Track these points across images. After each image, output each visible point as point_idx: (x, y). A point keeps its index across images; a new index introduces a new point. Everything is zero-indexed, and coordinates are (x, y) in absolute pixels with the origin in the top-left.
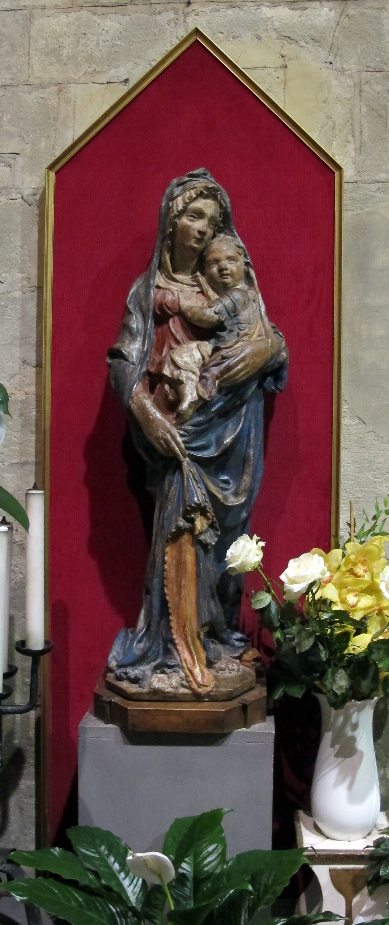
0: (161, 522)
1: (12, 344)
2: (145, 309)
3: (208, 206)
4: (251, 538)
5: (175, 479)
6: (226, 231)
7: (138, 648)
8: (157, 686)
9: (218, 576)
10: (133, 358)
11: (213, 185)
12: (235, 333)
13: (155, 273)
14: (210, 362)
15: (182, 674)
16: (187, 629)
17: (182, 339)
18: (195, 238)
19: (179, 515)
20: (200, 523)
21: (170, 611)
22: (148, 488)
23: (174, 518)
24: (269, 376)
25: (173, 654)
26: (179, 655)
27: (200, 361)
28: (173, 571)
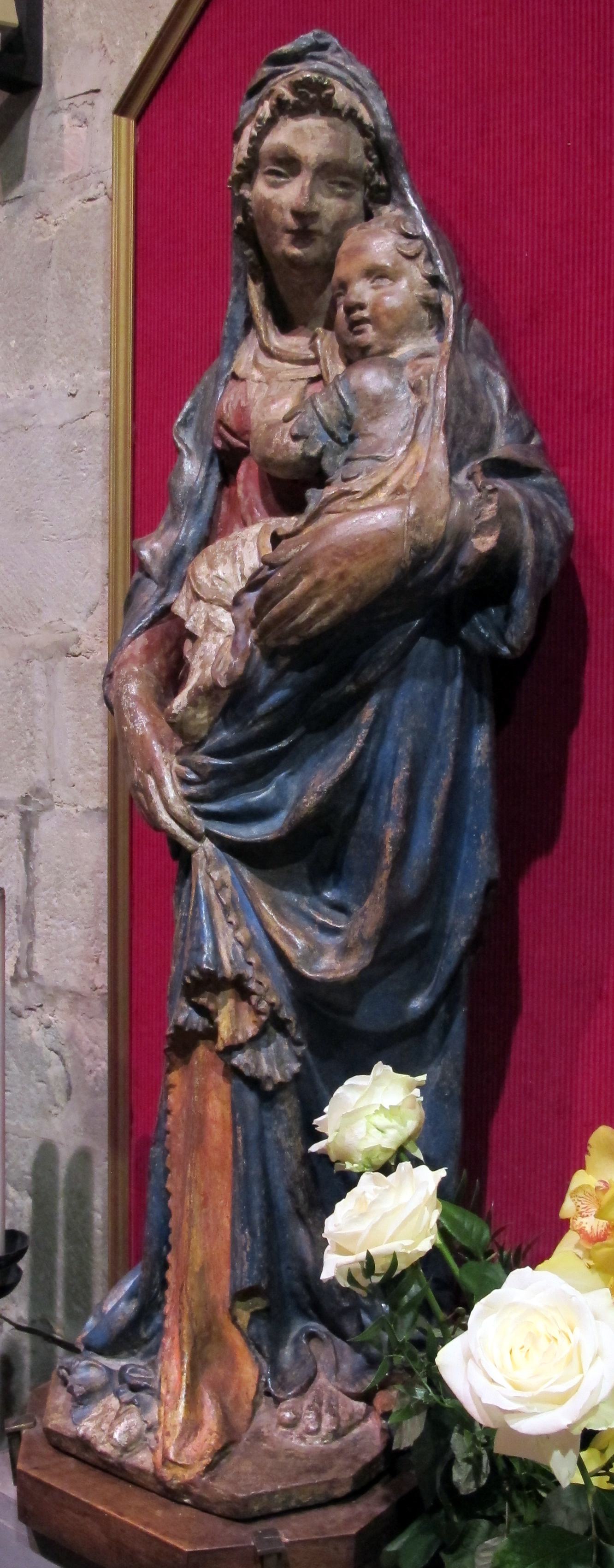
1: (90, 536)
20: (232, 1021)
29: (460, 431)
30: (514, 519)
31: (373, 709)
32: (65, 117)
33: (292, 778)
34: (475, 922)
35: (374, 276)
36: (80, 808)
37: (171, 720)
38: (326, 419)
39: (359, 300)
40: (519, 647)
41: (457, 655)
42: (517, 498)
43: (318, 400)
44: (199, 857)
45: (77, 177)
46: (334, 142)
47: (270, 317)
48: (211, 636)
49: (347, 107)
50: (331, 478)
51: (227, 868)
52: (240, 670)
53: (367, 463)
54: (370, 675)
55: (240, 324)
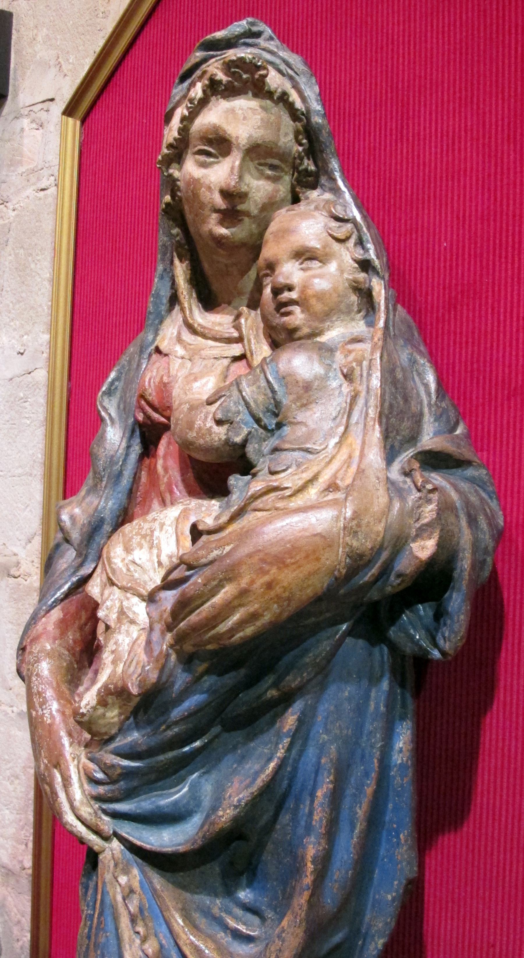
1: (31, 475)
29: (393, 420)
30: (452, 519)
31: (295, 717)
32: (25, 122)
33: (206, 776)
34: (393, 924)
36: (15, 709)
37: (78, 718)
38: (252, 404)
39: (288, 282)
40: (451, 652)
41: (382, 653)
42: (454, 495)
43: (244, 384)
44: (105, 858)
45: (33, 171)
46: (266, 124)
47: (194, 295)
48: (124, 628)
49: (280, 90)
50: (257, 469)
51: (135, 871)
52: (153, 677)
53: (296, 454)
54: (293, 681)
55: (165, 301)
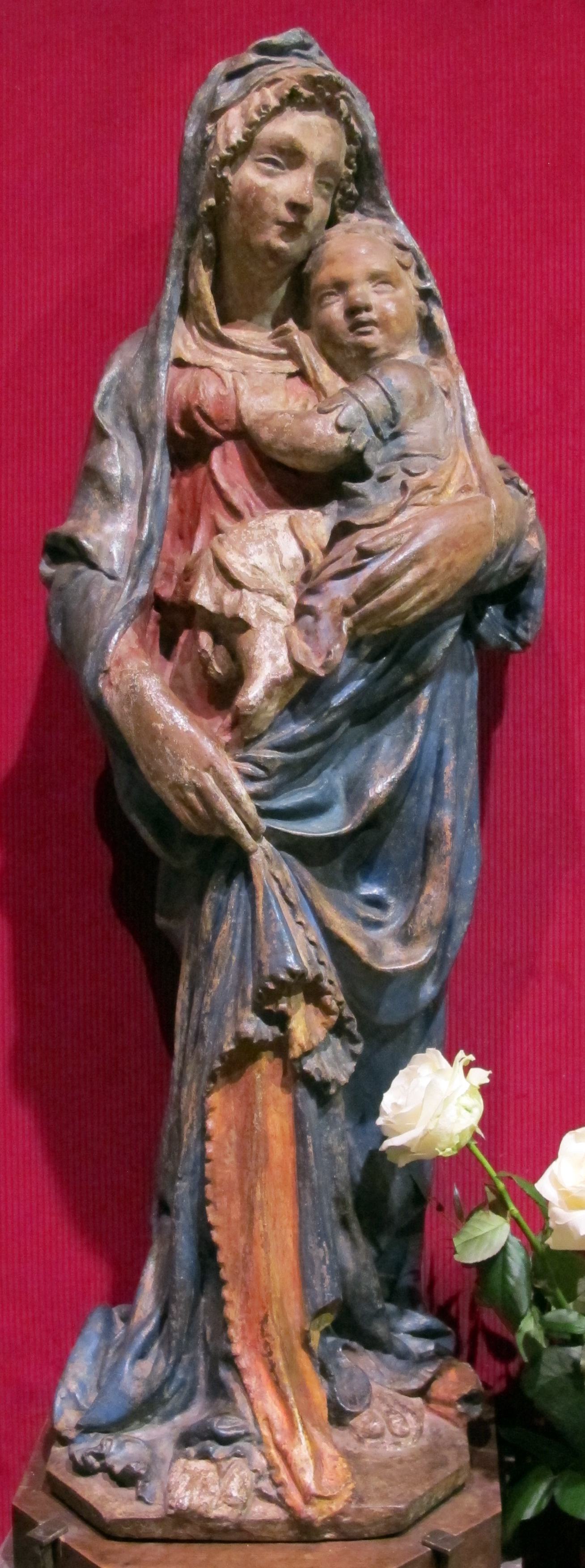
0: (194, 1021)
2: (143, 426)
3: (313, 132)
4: (451, 1060)
5: (233, 901)
6: (366, 205)
7: (136, 1376)
8: (186, 1503)
9: (360, 1160)
10: (112, 560)
11: (327, 73)
12: (396, 481)
13: (172, 326)
14: (325, 567)
15: (260, 1461)
16: (271, 1328)
17: (248, 505)
18: (279, 222)
19: (244, 1005)
20: (305, 1024)
21: (224, 1274)
22: (161, 921)
23: (229, 1011)
24: (493, 604)
25: (234, 1401)
26: (251, 1404)
27: (296, 566)
28: (230, 1160)
35: (378, 281)
38: (373, 414)
